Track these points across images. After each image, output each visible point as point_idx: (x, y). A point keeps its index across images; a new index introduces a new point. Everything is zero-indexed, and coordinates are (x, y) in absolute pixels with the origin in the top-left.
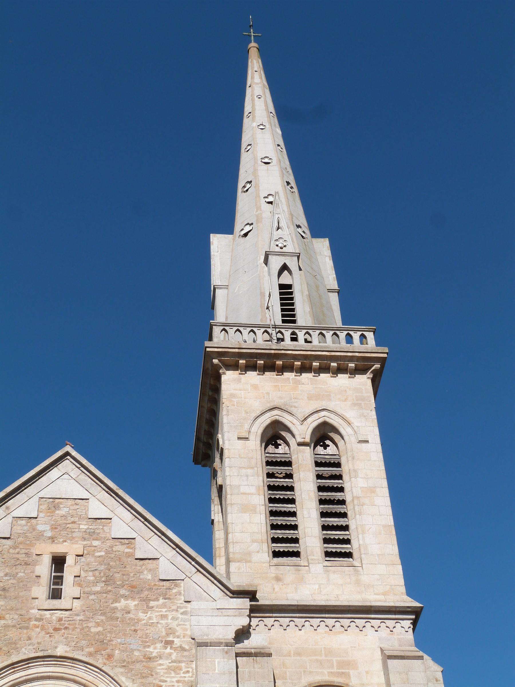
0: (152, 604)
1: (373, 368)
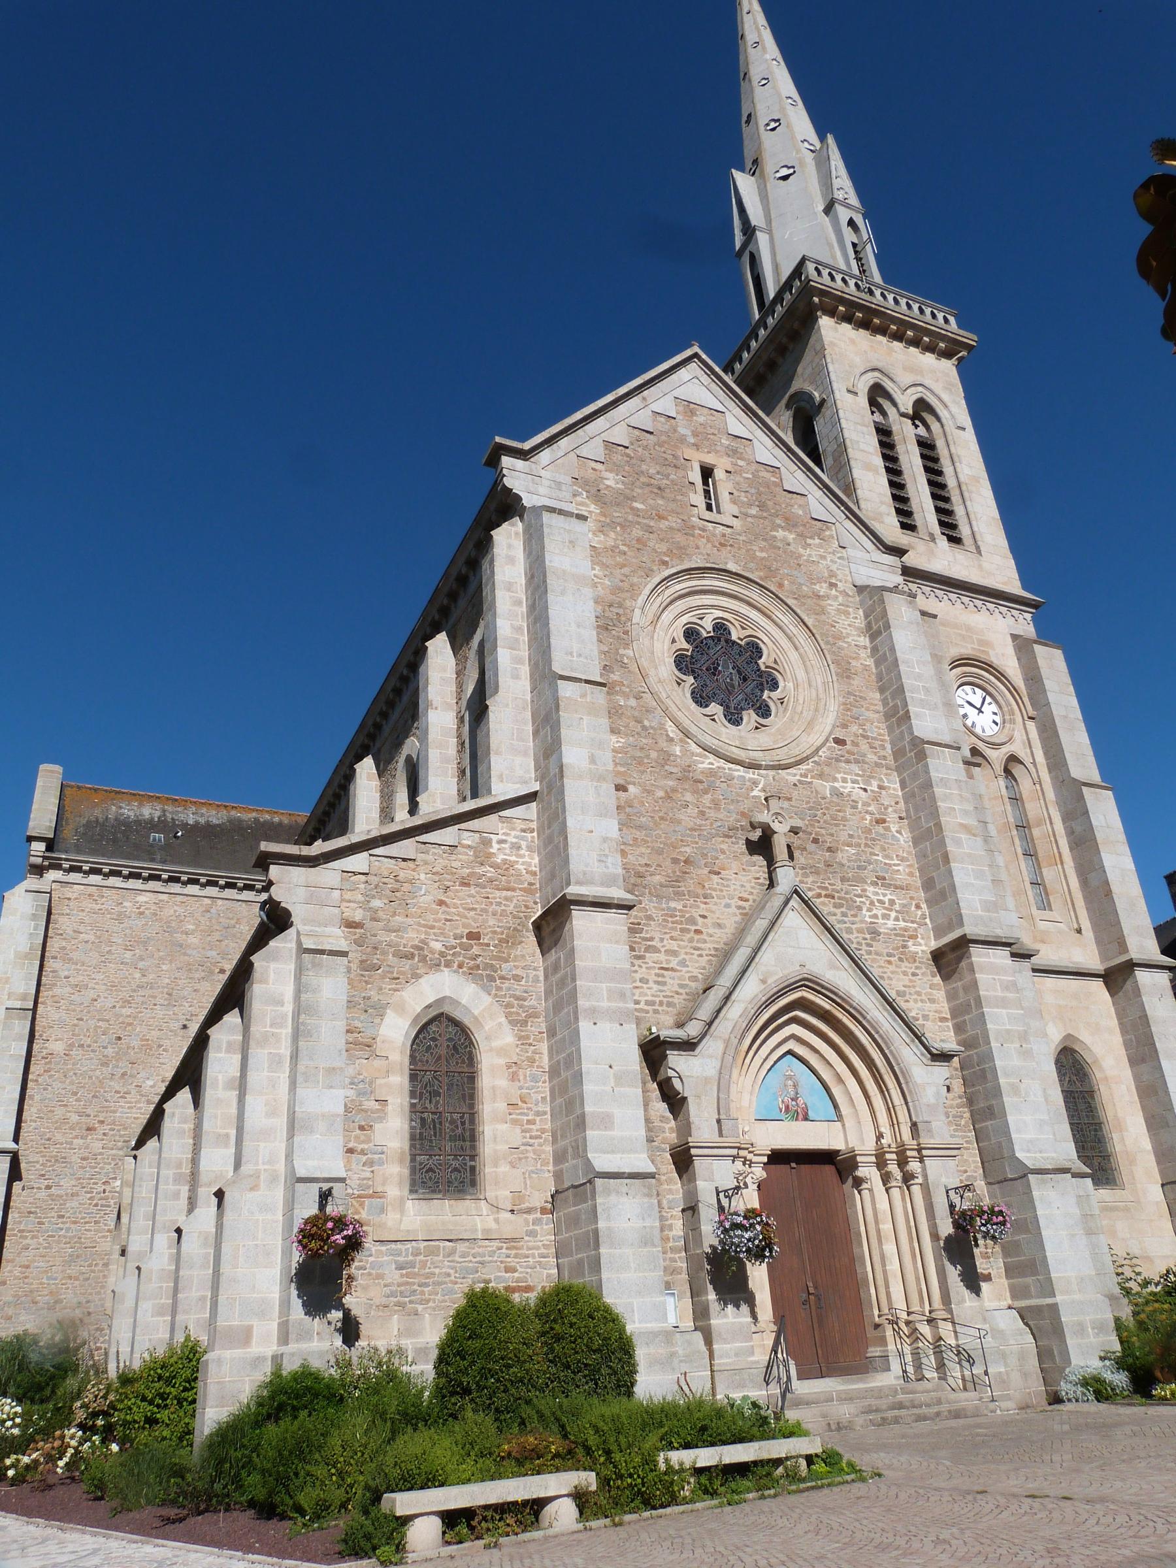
0: (809, 541)
1: (960, 355)
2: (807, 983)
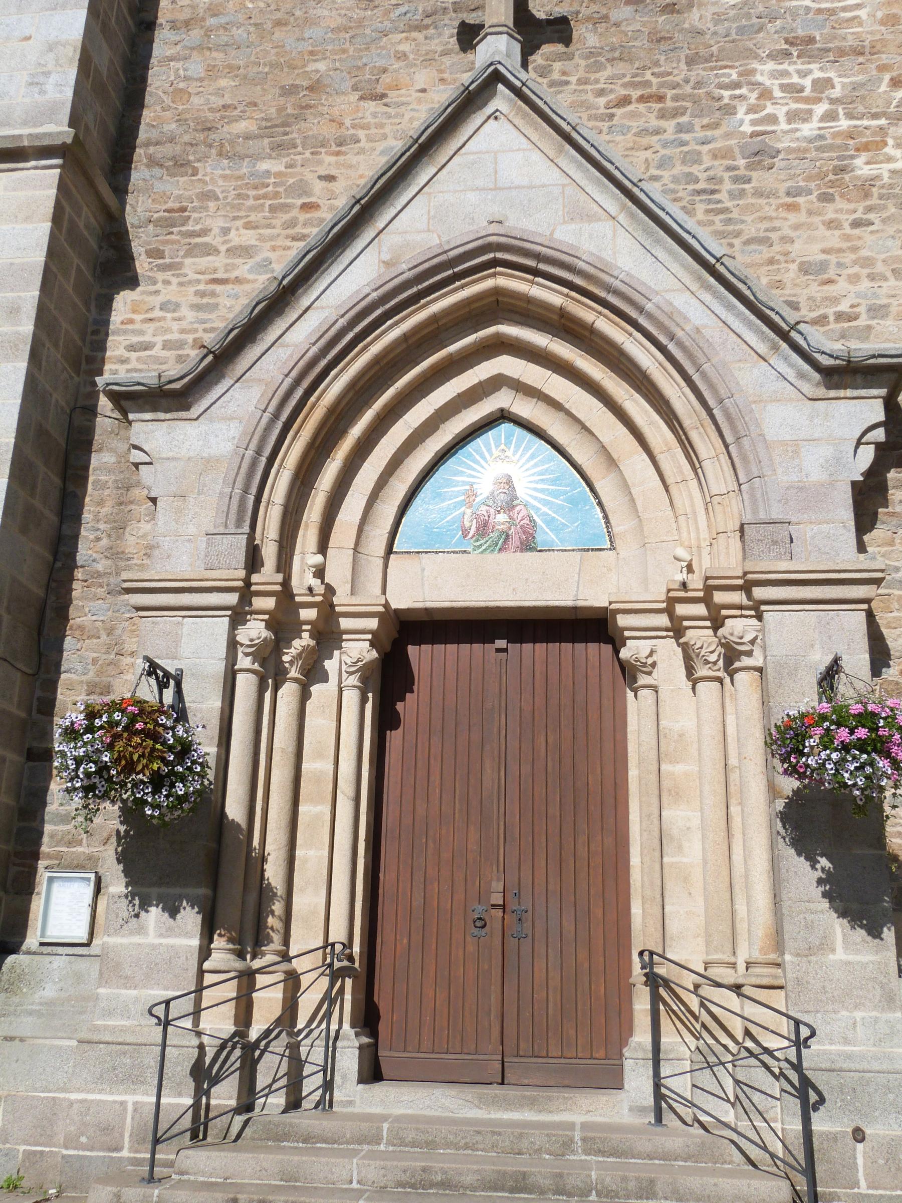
2: (499, 255)
